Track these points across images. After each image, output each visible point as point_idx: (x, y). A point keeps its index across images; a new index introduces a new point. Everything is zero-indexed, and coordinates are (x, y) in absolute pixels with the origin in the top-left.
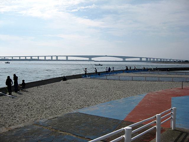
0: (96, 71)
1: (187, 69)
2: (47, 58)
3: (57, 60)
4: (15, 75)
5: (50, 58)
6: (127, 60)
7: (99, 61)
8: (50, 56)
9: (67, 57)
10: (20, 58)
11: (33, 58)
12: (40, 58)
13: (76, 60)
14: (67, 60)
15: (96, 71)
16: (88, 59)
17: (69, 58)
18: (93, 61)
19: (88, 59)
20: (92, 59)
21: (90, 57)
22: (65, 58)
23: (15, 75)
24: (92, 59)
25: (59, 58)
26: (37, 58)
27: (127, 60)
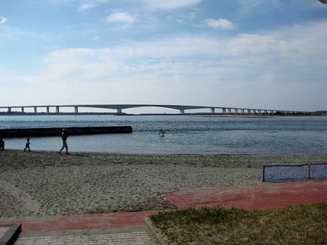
0: (64, 140)
1: (96, 131)
2: (39, 110)
3: (58, 113)
4: (20, 227)
5: (44, 110)
6: (186, 111)
7: (134, 115)
8: (32, 107)
9: (76, 107)
10: (23, 110)
11: (13, 110)
12: (26, 110)
13: (91, 114)
14: (76, 113)
15: (64, 140)
16: (115, 111)
17: (80, 110)
18: (125, 114)
19: (115, 111)
20: (123, 111)
21: (119, 107)
22: (72, 110)
23: (20, 227)
24: (123, 111)
25: (61, 110)
26: (20, 110)
27: (186, 111)
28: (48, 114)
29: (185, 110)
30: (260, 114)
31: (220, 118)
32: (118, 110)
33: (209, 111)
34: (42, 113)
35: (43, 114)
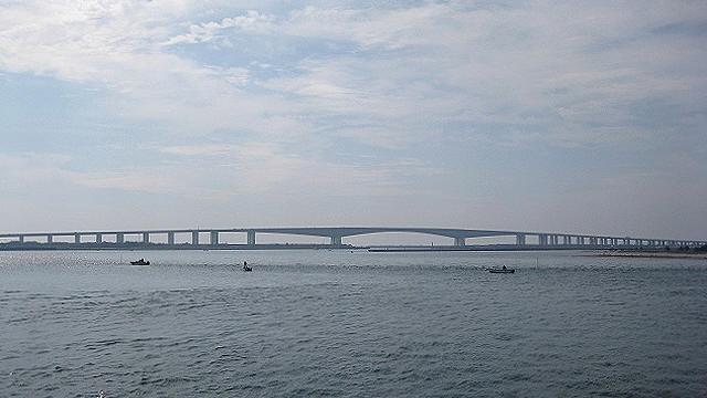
2: (179, 239)
3: (215, 246)
6: (469, 241)
9: (251, 232)
14: (252, 246)
16: (328, 241)
17: (260, 239)
20: (345, 240)
21: (336, 233)
22: (243, 239)
24: (345, 240)
25: (222, 239)
28: (195, 246)
29: (466, 239)
30: (635, 249)
31: (669, 261)
32: (457, 239)
33: (513, 240)
34: (159, 244)
35: (160, 247)
